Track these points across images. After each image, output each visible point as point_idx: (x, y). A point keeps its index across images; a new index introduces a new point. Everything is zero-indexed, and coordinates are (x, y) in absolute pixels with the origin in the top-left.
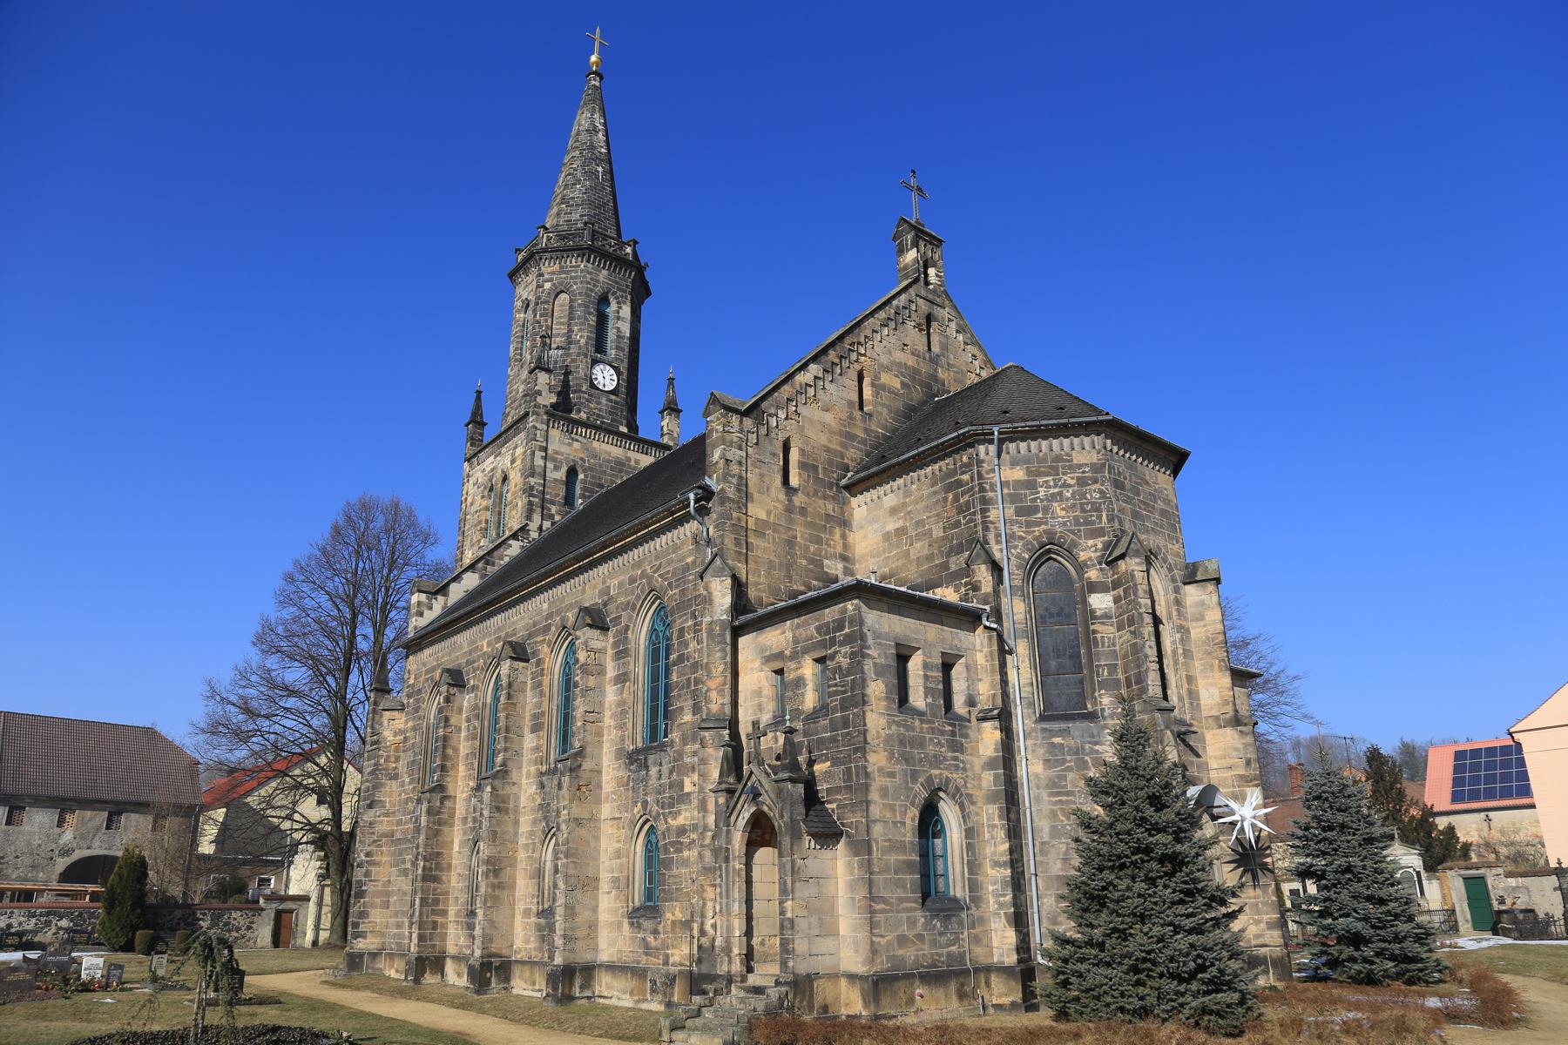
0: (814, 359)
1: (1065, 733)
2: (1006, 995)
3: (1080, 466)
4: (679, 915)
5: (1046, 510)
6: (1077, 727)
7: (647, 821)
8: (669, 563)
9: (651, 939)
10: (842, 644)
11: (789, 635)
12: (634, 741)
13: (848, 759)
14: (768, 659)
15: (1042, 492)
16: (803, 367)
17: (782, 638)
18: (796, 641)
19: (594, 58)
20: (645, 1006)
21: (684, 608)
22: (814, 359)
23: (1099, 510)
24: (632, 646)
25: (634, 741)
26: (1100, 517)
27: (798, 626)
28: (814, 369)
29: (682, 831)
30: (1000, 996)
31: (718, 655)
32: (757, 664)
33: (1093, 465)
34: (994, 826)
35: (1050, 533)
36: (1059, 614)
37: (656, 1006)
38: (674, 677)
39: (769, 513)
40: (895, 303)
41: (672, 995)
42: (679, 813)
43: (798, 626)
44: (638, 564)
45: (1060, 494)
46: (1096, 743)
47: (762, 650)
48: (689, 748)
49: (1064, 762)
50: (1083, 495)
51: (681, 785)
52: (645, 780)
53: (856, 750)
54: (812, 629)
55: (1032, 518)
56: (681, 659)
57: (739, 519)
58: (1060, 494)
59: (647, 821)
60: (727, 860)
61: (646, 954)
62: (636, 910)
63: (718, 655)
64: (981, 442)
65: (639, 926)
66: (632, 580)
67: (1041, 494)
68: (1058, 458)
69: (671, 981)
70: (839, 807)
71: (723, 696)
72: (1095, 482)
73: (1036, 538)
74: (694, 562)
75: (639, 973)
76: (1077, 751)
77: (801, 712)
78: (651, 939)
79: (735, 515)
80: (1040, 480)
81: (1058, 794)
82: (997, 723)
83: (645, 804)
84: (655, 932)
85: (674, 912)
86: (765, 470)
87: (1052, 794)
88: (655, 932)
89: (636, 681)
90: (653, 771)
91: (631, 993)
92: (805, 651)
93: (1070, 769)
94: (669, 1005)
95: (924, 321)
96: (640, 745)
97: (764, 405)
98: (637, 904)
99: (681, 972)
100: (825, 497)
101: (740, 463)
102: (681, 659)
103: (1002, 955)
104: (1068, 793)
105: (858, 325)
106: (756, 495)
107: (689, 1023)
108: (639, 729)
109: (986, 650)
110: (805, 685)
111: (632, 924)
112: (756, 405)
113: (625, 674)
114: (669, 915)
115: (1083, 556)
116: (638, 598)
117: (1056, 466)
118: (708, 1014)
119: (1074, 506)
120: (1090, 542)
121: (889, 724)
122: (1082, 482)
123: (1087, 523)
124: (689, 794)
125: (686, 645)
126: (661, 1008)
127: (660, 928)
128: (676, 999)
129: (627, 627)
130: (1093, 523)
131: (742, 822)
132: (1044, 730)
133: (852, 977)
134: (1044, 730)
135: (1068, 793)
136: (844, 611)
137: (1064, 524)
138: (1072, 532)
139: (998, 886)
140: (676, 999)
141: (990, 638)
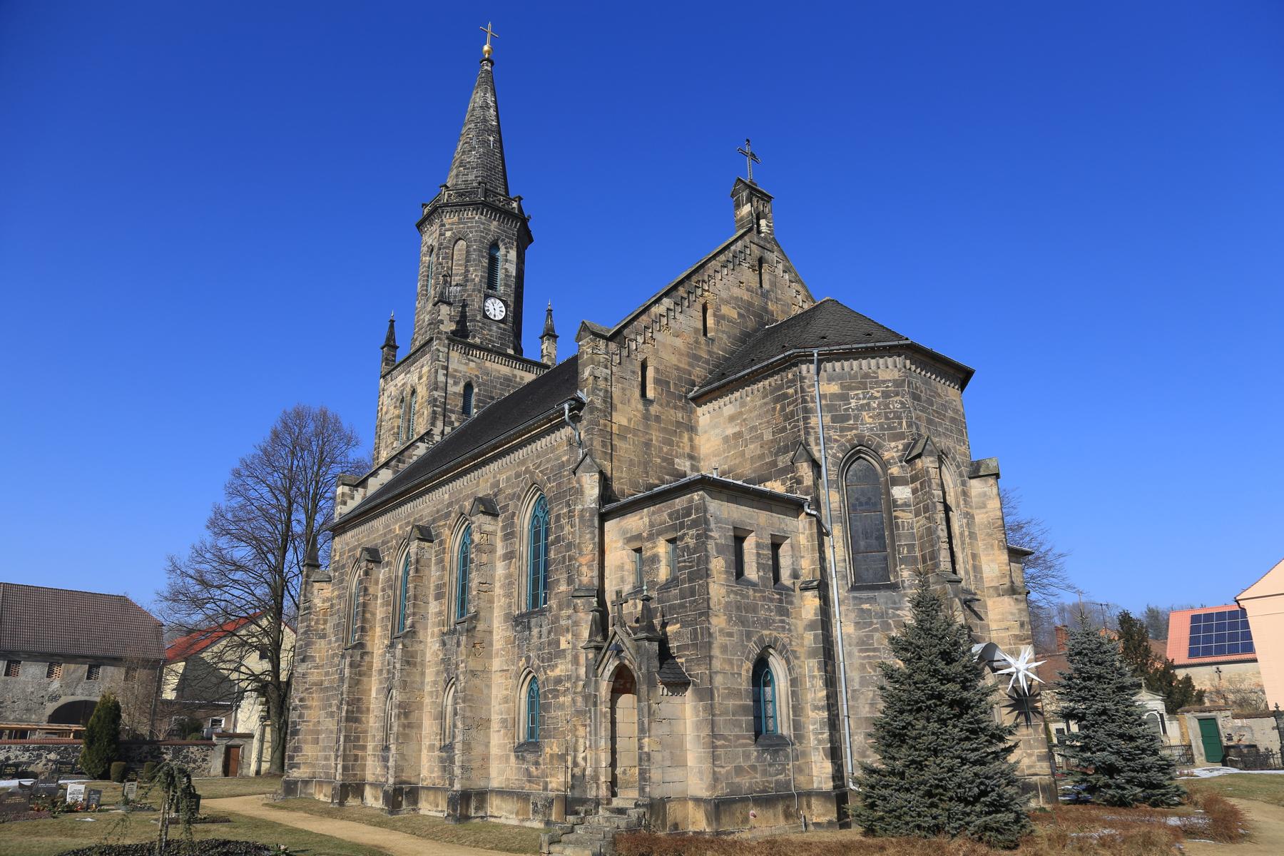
0: (667, 294)
1: (872, 600)
2: (824, 815)
3: (884, 382)
4: (556, 750)
5: (856, 418)
6: (882, 596)
7: (530, 672)
8: (548, 461)
9: (533, 769)
10: (690, 528)
11: (646, 520)
12: (519, 607)
13: (695, 622)
14: (629, 540)
15: (853, 403)
16: (658, 301)
17: (640, 522)
18: (652, 525)
19: (486, 48)
20: (528, 824)
21: (560, 498)
22: (667, 294)
23: (900, 418)
24: (517, 529)
25: (519, 607)
26: (900, 424)
27: (654, 513)
28: (667, 302)
29: (558, 681)
30: (819, 816)
31: (588, 536)
32: (620, 544)
33: (895, 381)
34: (814, 677)
35: (860, 437)
36: (867, 503)
37: (537, 824)
38: (552, 555)
39: (630, 420)
40: (733, 248)
41: (550, 815)
42: (556, 666)
43: (654, 513)
44: (523, 462)
45: (868, 404)
46: (898, 609)
47: (625, 532)
48: (564, 613)
49: (871, 624)
50: (887, 406)
51: (558, 643)
52: (528, 639)
53: (701, 614)
54: (665, 516)
55: (845, 425)
56: (558, 539)
57: (605, 425)
58: (868, 404)
59: (530, 672)
60: (595, 705)
61: (529, 781)
62: (520, 745)
63: (588, 536)
64: (803, 362)
65: (524, 759)
66: (518, 475)
67: (853, 405)
68: (866, 376)
69: (549, 803)
70: (687, 661)
71: (592, 570)
72: (897, 395)
73: (848, 441)
74: (568, 461)
75: (523, 797)
76: (882, 615)
77: (656, 583)
78: (533, 769)
79: (602, 421)
80: (852, 393)
81: (867, 650)
82: (816, 593)
83: (528, 659)
84: (537, 763)
85: (552, 747)
86: (626, 385)
87: (861, 651)
88: (537, 763)
89: (521, 558)
90: (535, 631)
91: (517, 814)
92: (660, 533)
93: (876, 630)
94: (548, 823)
95: (756, 263)
96: (524, 610)
97: (625, 332)
98: (522, 740)
99: (557, 796)
100: (675, 407)
101: (606, 379)
102: (558, 539)
103: (820, 782)
104: (875, 650)
105: (702, 266)
106: (619, 406)
107: (564, 838)
108: (523, 597)
109: (807, 532)
110: (659, 561)
111: (517, 757)
112: (619, 332)
113: (512, 552)
114: (547, 750)
115: (887, 455)
116: (522, 490)
117: (865, 381)
118: (580, 831)
119: (879, 414)
120: (893, 444)
121: (728, 593)
122: (886, 395)
123: (890, 428)
124: (564, 650)
125: (562, 528)
126: (542, 826)
127: (541, 760)
128: (553, 818)
129: (514, 514)
130: (895, 428)
131: (607, 674)
132: (855, 598)
133: (698, 801)
134: (855, 598)
135: (875, 650)
136: (692, 500)
137: (872, 429)
138: (878, 436)
139: (818, 726)
140: (553, 818)
141: (811, 523)
